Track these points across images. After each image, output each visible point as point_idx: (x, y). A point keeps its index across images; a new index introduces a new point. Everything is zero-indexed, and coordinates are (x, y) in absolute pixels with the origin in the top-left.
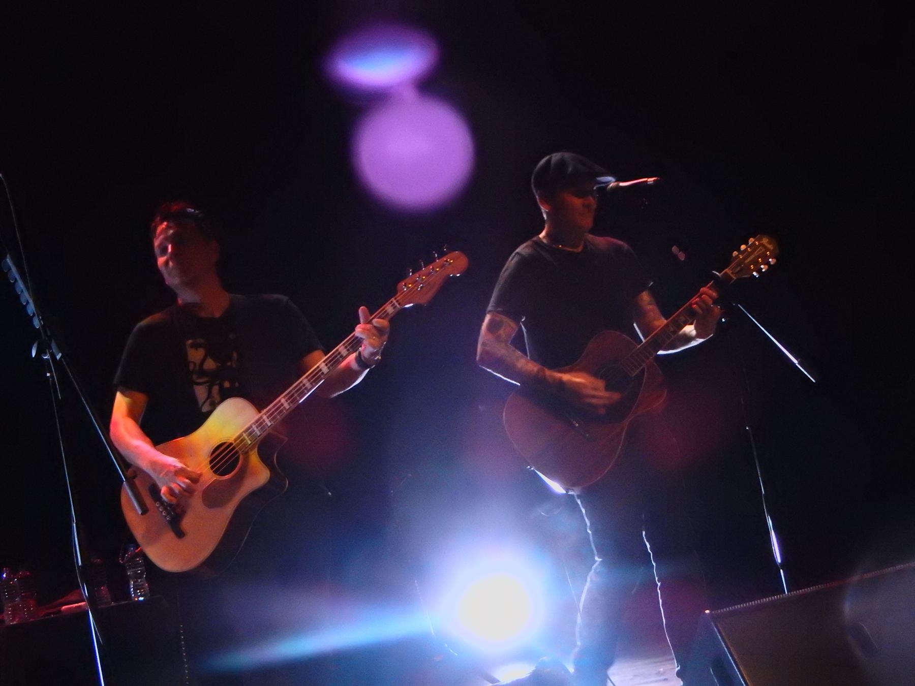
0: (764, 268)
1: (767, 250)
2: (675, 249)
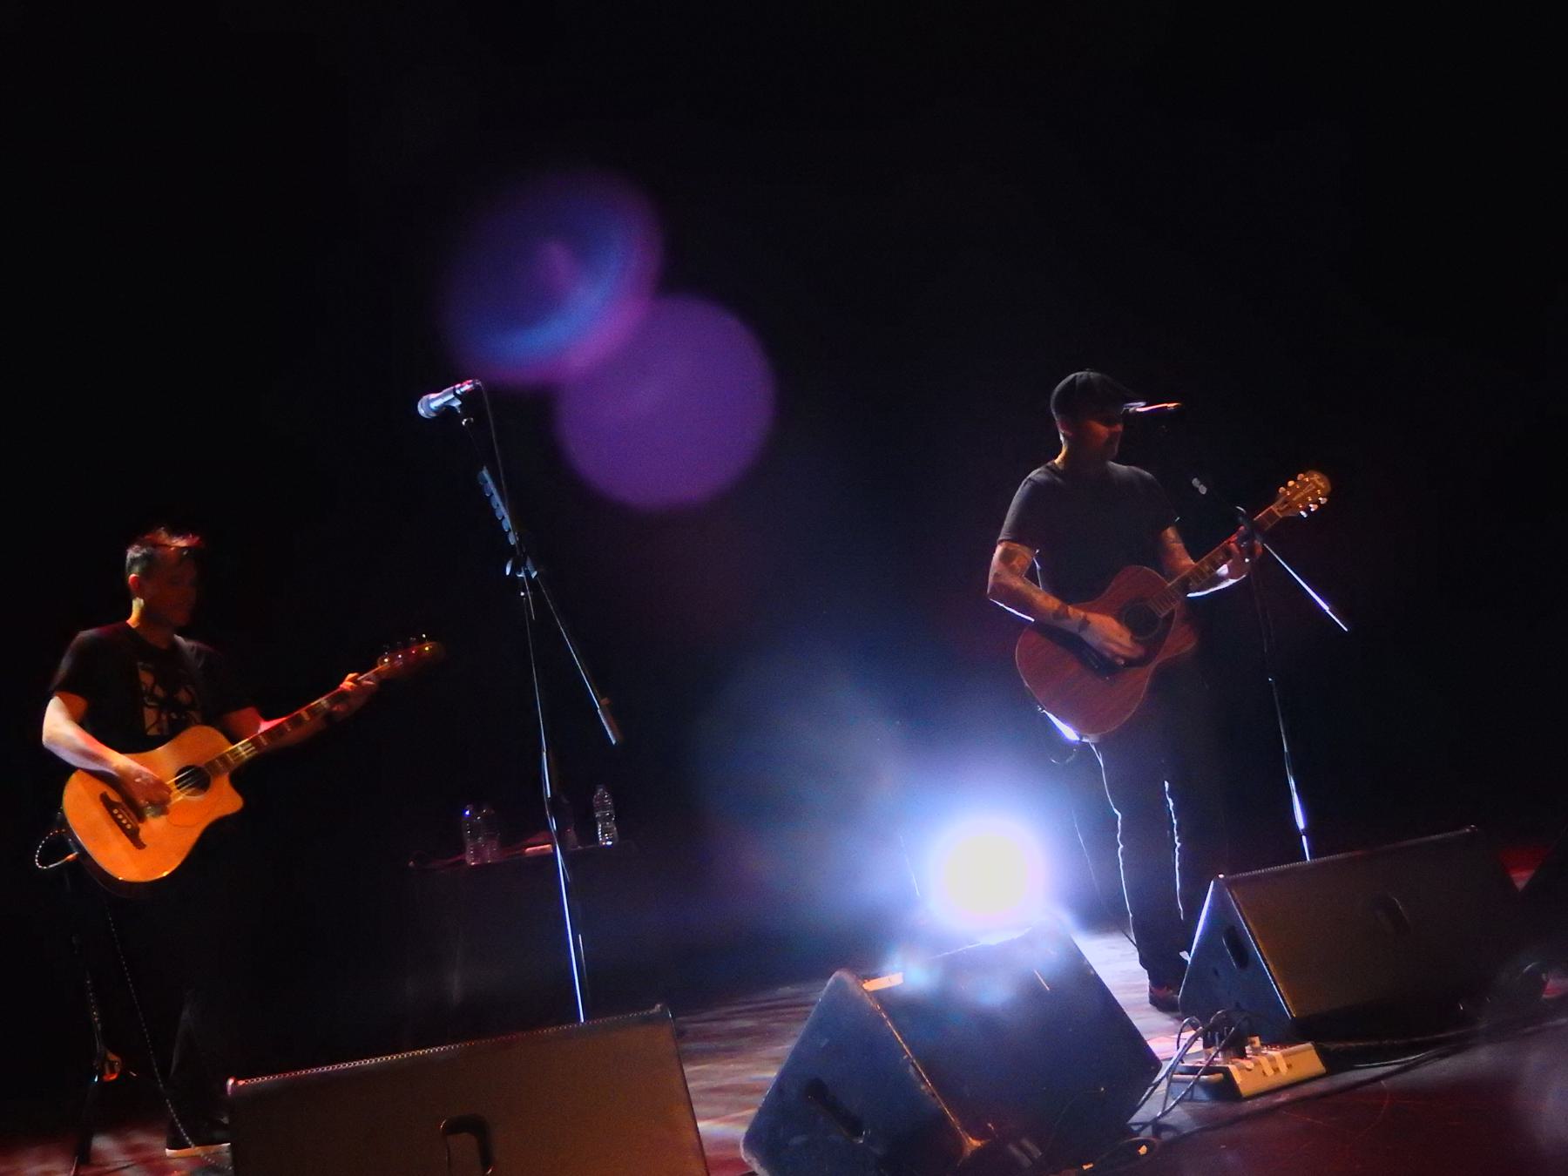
0: (1313, 508)
1: (1318, 487)
2: (1195, 482)
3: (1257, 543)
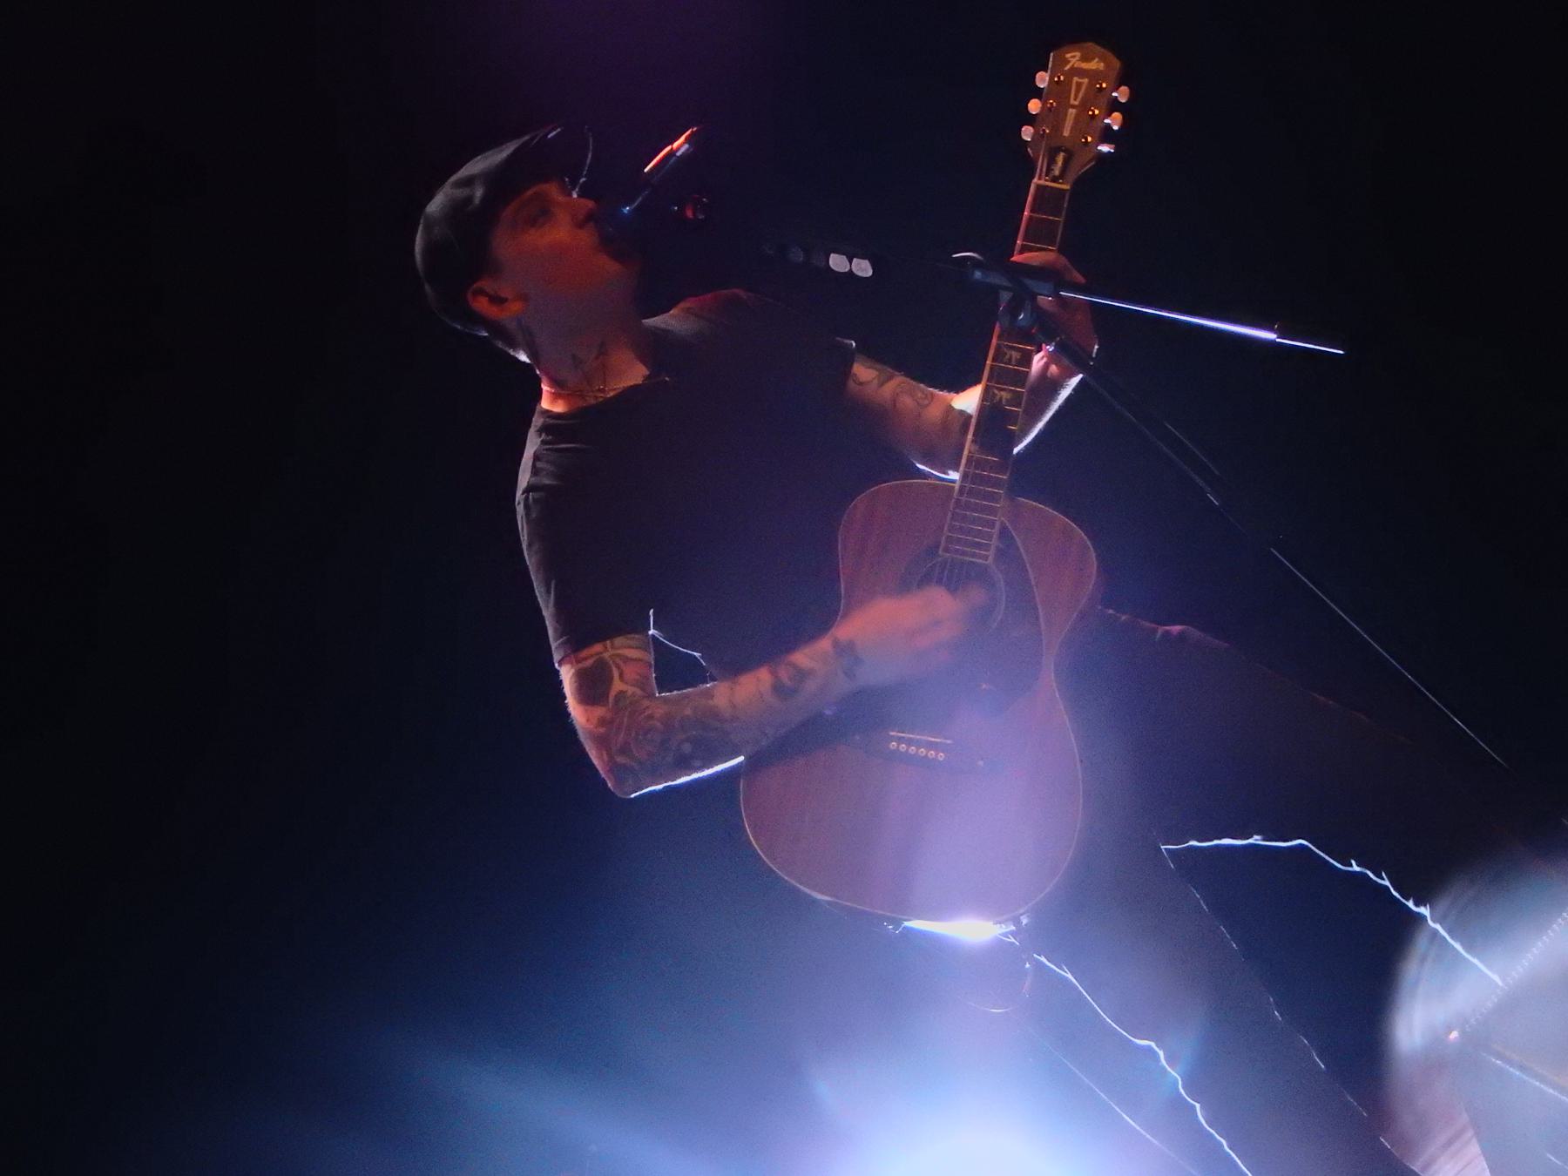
0: (1115, 121)
1: (1094, 76)
2: (837, 262)
3: (1045, 301)
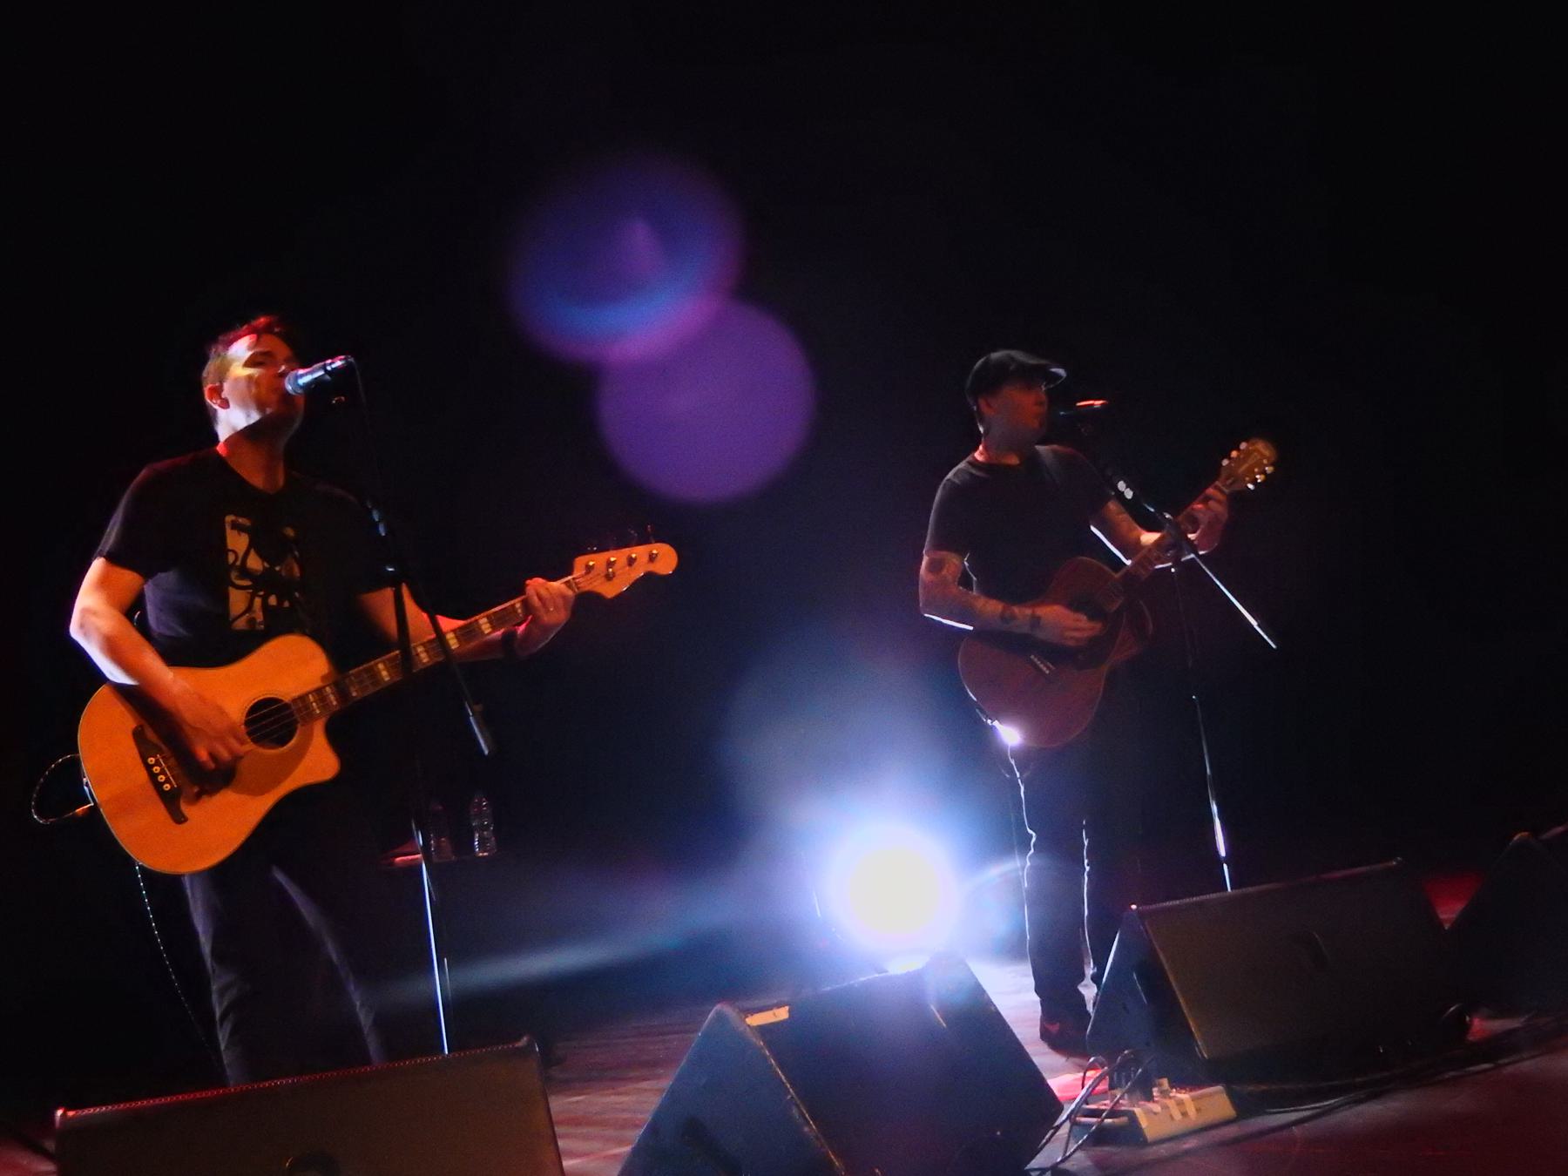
0: (1260, 478)
1: (1264, 457)
2: (1121, 485)
